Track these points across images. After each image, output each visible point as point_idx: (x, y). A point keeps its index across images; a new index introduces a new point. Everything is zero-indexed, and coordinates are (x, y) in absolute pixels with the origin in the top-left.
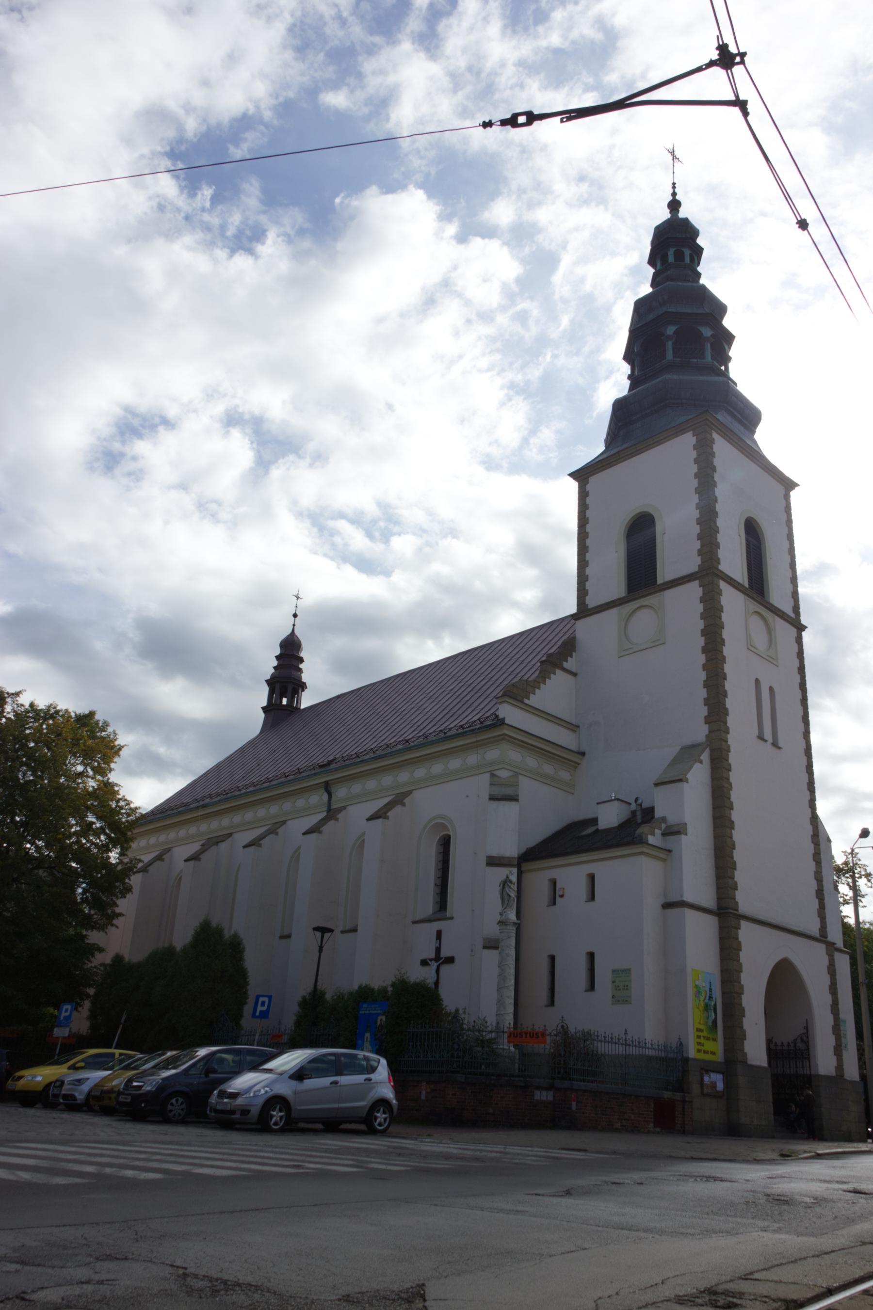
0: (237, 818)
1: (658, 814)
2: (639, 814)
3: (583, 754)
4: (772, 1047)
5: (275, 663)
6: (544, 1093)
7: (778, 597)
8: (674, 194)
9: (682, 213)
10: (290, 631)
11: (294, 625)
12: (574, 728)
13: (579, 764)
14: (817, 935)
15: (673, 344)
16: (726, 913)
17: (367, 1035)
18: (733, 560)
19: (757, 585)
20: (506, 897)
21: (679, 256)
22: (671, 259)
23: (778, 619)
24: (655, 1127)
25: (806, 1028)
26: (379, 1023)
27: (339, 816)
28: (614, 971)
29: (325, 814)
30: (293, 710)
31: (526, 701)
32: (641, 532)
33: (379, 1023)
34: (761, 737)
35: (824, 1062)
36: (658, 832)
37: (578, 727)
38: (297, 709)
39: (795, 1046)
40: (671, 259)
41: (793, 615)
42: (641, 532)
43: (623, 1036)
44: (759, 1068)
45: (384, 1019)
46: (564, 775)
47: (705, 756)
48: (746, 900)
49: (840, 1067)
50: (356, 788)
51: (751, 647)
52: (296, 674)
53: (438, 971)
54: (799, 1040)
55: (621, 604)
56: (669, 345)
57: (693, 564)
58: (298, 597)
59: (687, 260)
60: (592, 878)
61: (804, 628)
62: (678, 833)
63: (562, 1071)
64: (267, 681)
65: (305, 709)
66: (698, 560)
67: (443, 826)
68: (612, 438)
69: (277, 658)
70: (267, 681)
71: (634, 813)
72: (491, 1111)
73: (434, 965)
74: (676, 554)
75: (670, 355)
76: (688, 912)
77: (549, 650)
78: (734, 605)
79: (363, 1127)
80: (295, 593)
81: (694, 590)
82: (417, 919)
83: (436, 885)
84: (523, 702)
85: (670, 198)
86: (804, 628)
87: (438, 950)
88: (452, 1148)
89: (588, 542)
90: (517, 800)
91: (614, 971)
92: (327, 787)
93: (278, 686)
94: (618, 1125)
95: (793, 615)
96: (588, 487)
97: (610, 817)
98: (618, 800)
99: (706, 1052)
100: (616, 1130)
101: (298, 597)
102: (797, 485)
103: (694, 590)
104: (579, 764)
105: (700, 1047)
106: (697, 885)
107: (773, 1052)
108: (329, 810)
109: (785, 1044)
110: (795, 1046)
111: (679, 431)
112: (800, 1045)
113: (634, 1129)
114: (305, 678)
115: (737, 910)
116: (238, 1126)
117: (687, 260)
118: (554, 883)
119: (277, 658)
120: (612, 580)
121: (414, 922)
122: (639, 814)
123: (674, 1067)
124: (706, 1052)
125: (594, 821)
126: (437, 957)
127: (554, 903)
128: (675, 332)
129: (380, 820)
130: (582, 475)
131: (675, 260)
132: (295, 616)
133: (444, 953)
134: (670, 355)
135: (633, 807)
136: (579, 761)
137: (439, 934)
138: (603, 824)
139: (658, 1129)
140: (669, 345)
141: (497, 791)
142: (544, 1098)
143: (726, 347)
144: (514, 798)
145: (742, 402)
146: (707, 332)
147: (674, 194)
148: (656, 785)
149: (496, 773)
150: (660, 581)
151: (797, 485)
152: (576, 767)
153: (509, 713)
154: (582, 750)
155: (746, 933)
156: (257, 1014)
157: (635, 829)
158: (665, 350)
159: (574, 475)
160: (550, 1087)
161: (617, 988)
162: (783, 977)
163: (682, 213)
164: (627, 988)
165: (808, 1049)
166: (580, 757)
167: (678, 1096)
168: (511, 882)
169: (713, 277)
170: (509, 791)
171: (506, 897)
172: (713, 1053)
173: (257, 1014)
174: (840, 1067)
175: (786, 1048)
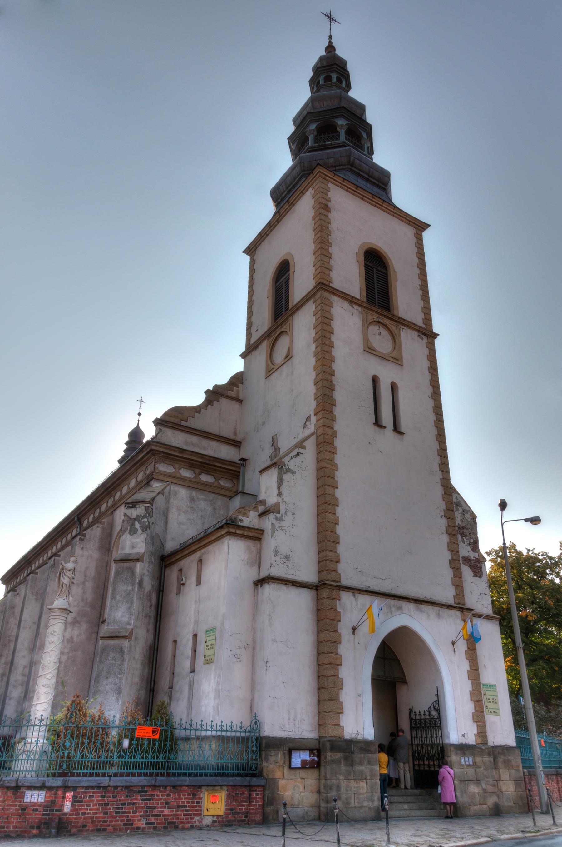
4: (412, 716)
6: (36, 793)
8: (330, 43)
10: (136, 425)
11: (139, 421)
12: (236, 444)
14: (451, 602)
25: (437, 695)
34: (378, 423)
35: (458, 728)
39: (430, 715)
48: (348, 574)
49: (482, 734)
54: (432, 709)
61: (436, 335)
69: (126, 444)
80: (139, 399)
86: (436, 335)
94: (142, 823)
101: (141, 401)
109: (422, 713)
110: (430, 715)
115: (339, 582)
119: (126, 444)
131: (325, 82)
132: (139, 414)
142: (34, 800)
147: (330, 43)
165: (439, 717)
175: (423, 717)
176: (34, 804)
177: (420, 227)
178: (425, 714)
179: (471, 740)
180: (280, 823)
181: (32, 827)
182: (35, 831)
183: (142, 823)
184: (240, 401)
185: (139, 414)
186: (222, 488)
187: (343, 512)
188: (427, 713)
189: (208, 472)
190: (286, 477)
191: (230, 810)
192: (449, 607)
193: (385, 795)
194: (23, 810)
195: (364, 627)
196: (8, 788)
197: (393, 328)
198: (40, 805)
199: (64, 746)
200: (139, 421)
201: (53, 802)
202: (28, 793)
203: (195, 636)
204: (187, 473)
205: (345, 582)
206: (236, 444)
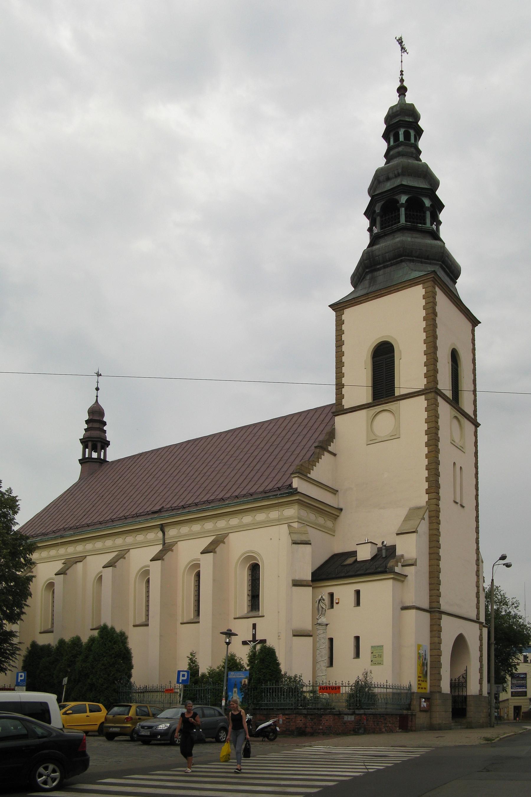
0: (89, 546)
1: (399, 552)
2: (384, 552)
3: (341, 510)
5: (86, 426)
6: (350, 717)
7: (467, 406)
8: (402, 81)
11: (97, 396)
13: (338, 516)
15: (406, 210)
20: (320, 609)
22: (401, 138)
23: (466, 420)
24: (399, 729)
26: (243, 683)
27: (174, 548)
28: (372, 647)
29: (160, 547)
30: (102, 462)
31: (309, 475)
32: (383, 356)
33: (243, 683)
37: (338, 491)
38: (104, 461)
39: (459, 680)
40: (401, 138)
41: (473, 417)
42: (383, 356)
43: (385, 684)
44: (447, 694)
45: (247, 682)
46: (329, 524)
50: (185, 529)
51: (453, 443)
54: (461, 677)
55: (368, 408)
57: (421, 383)
59: (412, 140)
60: (358, 592)
63: (358, 705)
64: (80, 439)
65: (113, 462)
66: (425, 381)
67: (254, 558)
68: (357, 279)
70: (80, 439)
71: (380, 550)
72: (321, 727)
74: (409, 373)
79: (214, 740)
82: (237, 616)
83: (248, 595)
84: (307, 476)
85: (398, 84)
87: (254, 636)
88: (348, 750)
89: (344, 359)
90: (310, 544)
91: (372, 647)
92: (162, 528)
93: (90, 444)
95: (473, 417)
96: (344, 317)
97: (365, 554)
98: (371, 542)
99: (422, 688)
100: (383, 732)
103: (421, 402)
104: (338, 516)
105: (420, 686)
107: (454, 685)
108: (164, 544)
110: (459, 680)
111: (412, 283)
112: (462, 680)
113: (390, 731)
114: (109, 437)
115: (440, 609)
117: (412, 140)
118: (332, 595)
119: (87, 422)
120: (359, 390)
121: (235, 619)
122: (384, 552)
124: (422, 688)
125: (354, 554)
126: (254, 639)
127: (332, 607)
128: (406, 201)
129: (212, 554)
130: (339, 307)
132: (97, 389)
133: (258, 638)
135: (380, 545)
136: (338, 514)
137: (254, 626)
139: (400, 730)
141: (297, 538)
142: (349, 719)
143: (438, 214)
144: (307, 543)
145: (451, 261)
146: (427, 203)
147: (402, 81)
148: (398, 534)
149: (290, 524)
152: (336, 518)
153: (296, 483)
154: (340, 507)
155: (445, 621)
156: (181, 681)
157: (383, 563)
158: (399, 215)
161: (374, 656)
163: (409, 99)
164: (380, 656)
165: (466, 681)
166: (339, 511)
167: (409, 712)
168: (324, 600)
169: (431, 151)
170: (304, 538)
171: (320, 609)
172: (425, 688)
173: (181, 681)
176: (349, 722)
177: (475, 322)
178: (455, 680)
180: (177, 745)
181: (350, 731)
182: (352, 732)
185: (97, 389)
188: (457, 680)
193: (506, 717)
194: (345, 724)
196: (335, 714)
198: (352, 722)
199: (357, 696)
200: (97, 396)
201: (360, 720)
202: (346, 717)
206: (334, 492)
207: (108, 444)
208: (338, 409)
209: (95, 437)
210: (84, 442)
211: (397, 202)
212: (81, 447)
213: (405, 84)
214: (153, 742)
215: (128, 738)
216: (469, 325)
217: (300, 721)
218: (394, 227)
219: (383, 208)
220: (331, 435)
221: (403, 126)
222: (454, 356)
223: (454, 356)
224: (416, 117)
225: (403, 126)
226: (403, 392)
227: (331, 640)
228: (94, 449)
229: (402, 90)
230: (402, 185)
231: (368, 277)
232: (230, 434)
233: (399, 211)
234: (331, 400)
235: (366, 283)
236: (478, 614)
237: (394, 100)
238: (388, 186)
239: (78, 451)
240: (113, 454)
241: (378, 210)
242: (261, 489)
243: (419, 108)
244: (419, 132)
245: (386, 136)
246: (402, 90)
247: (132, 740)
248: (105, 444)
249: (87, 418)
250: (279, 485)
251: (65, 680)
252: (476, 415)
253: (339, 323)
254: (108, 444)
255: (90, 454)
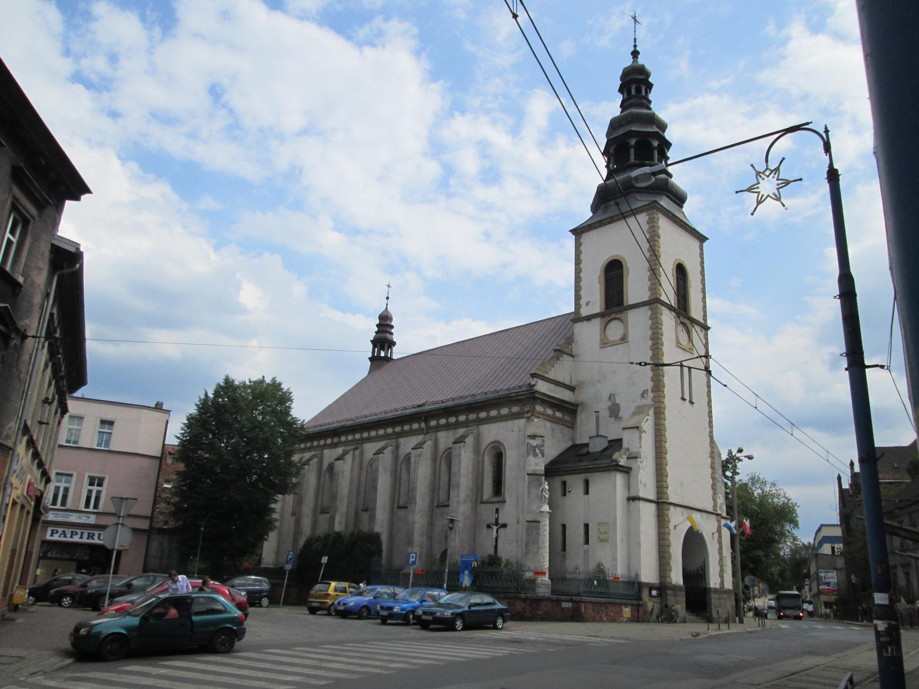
1: (625, 445)
5: (376, 329)
8: (635, 46)
9: (641, 60)
12: (572, 389)
14: (711, 510)
16: (661, 504)
17: (466, 572)
18: (668, 294)
19: (682, 309)
21: (638, 90)
22: (633, 92)
30: (388, 359)
32: (614, 271)
34: (683, 399)
35: (714, 581)
36: (625, 457)
38: (391, 359)
40: (633, 92)
42: (614, 271)
47: (651, 412)
48: (673, 496)
49: (722, 583)
51: (678, 345)
52: (389, 336)
53: (497, 531)
56: (632, 151)
58: (389, 286)
59: (644, 94)
62: (636, 458)
66: (649, 293)
68: (595, 207)
73: (495, 528)
74: (636, 289)
75: (632, 160)
76: (641, 503)
77: (558, 337)
78: (668, 320)
81: (645, 312)
85: (633, 49)
87: (497, 520)
93: (378, 345)
96: (582, 240)
101: (389, 286)
102: (707, 239)
106: (647, 489)
107: (686, 575)
112: (701, 572)
114: (395, 338)
116: (432, 626)
117: (644, 94)
120: (595, 302)
123: (635, 587)
127: (565, 495)
130: (578, 232)
132: (388, 298)
133: (501, 521)
134: (632, 160)
138: (592, 449)
140: (632, 151)
147: (635, 46)
150: (625, 304)
151: (707, 239)
159: (574, 231)
160: (571, 601)
162: (693, 540)
163: (641, 60)
174: (722, 583)
177: (702, 239)
179: (718, 586)
183: (605, 619)
184: (573, 356)
185: (388, 298)
186: (566, 421)
187: (669, 458)
189: (559, 411)
190: (643, 435)
191: (632, 615)
192: (712, 513)
195: (679, 524)
197: (689, 325)
203: (587, 526)
204: (549, 411)
205: (671, 500)
207: (394, 344)
208: (577, 318)
209: (383, 339)
210: (375, 342)
211: (628, 144)
212: (371, 346)
213: (638, 49)
214: (389, 621)
215: (326, 612)
216: (695, 243)
217: (519, 606)
218: (625, 165)
219: (616, 150)
220: (570, 340)
221: (635, 83)
222: (681, 270)
223: (681, 270)
224: (648, 75)
225: (635, 83)
226: (631, 302)
227: (564, 526)
228: (382, 348)
229: (635, 54)
230: (631, 131)
231: (602, 207)
232: (558, 320)
233: (629, 151)
234: (571, 309)
235: (601, 211)
236: (715, 506)
237: (628, 62)
238: (621, 132)
239: (368, 349)
240: (397, 353)
241: (611, 151)
242: (506, 387)
243: (648, 67)
244: (650, 86)
245: (621, 90)
246: (635, 54)
247: (329, 614)
248: (392, 344)
249: (378, 322)
250: (521, 384)
251: (325, 560)
252: (705, 320)
253: (578, 245)
254: (394, 344)
255: (379, 353)
